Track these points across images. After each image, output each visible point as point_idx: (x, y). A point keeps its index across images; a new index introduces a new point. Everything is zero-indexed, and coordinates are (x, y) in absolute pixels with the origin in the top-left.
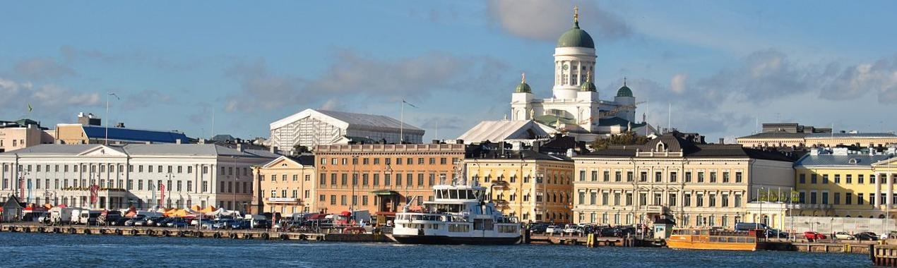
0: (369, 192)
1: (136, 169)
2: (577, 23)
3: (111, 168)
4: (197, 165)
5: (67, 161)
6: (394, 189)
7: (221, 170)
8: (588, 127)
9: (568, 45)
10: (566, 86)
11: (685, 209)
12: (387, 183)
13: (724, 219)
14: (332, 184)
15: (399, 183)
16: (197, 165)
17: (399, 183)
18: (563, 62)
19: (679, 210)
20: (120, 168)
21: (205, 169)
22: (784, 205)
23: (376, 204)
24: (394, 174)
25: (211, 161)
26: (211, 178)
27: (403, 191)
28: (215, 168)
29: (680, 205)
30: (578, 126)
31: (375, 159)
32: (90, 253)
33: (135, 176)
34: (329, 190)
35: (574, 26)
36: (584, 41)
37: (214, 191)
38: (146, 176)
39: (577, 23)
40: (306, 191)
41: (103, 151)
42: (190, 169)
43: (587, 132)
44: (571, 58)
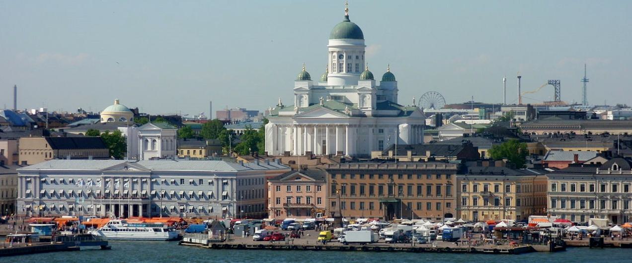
6: (397, 196)
23: (381, 208)
39: (347, 17)
40: (318, 198)
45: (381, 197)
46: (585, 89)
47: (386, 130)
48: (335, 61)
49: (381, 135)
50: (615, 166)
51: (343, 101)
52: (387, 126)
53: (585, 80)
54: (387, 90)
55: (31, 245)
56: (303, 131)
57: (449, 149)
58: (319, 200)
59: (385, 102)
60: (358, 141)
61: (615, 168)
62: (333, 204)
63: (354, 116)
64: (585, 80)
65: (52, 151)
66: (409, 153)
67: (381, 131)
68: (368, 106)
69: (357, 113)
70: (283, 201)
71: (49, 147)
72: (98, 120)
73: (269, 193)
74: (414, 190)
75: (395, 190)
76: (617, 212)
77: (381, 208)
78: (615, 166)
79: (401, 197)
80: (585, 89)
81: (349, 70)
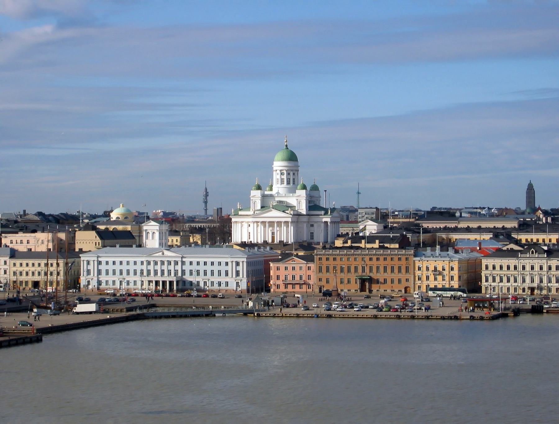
0: (353, 277)
1: (187, 263)
2: (287, 146)
3: (169, 263)
4: (232, 262)
5: (135, 259)
6: (368, 274)
7: (248, 264)
8: (304, 212)
9: (283, 160)
10: (283, 186)
11: (549, 285)
12: (363, 270)
13: (508, 289)
14: (348, 272)
15: (371, 270)
16: (232, 262)
17: (371, 270)
18: (281, 170)
19: (546, 285)
20: (176, 263)
21: (238, 264)
22: (50, 235)
23: (356, 283)
24: (368, 266)
25: (243, 260)
26: (243, 269)
27: (374, 275)
28: (245, 264)
29: (546, 282)
30: (297, 211)
31: (392, 258)
32: (169, 306)
33: (187, 268)
34: (324, 275)
35: (285, 147)
36: (292, 157)
37: (245, 276)
38: (194, 267)
39: (287, 146)
41: (163, 254)
42: (227, 264)
43: (303, 215)
44: (286, 168)
45: (356, 274)
46: (358, 198)
47: (315, 225)
48: (279, 177)
49: (312, 228)
50: (532, 251)
51: (285, 205)
52: (317, 222)
53: (359, 193)
54: (313, 197)
55: (108, 317)
56: (258, 226)
57: (26, 229)
58: (309, 277)
59: (313, 206)
60: (297, 233)
61: (533, 253)
62: (320, 280)
63: (294, 215)
64: (359, 193)
65: (100, 241)
66: (377, 241)
67: (312, 226)
68: (303, 209)
69: (296, 213)
70: (282, 278)
71: (98, 238)
72: (108, 218)
73: (271, 272)
74: (382, 269)
75: (367, 270)
76: (535, 285)
77: (356, 283)
78: (532, 251)
79: (371, 275)
80: (358, 198)
81: (288, 183)
